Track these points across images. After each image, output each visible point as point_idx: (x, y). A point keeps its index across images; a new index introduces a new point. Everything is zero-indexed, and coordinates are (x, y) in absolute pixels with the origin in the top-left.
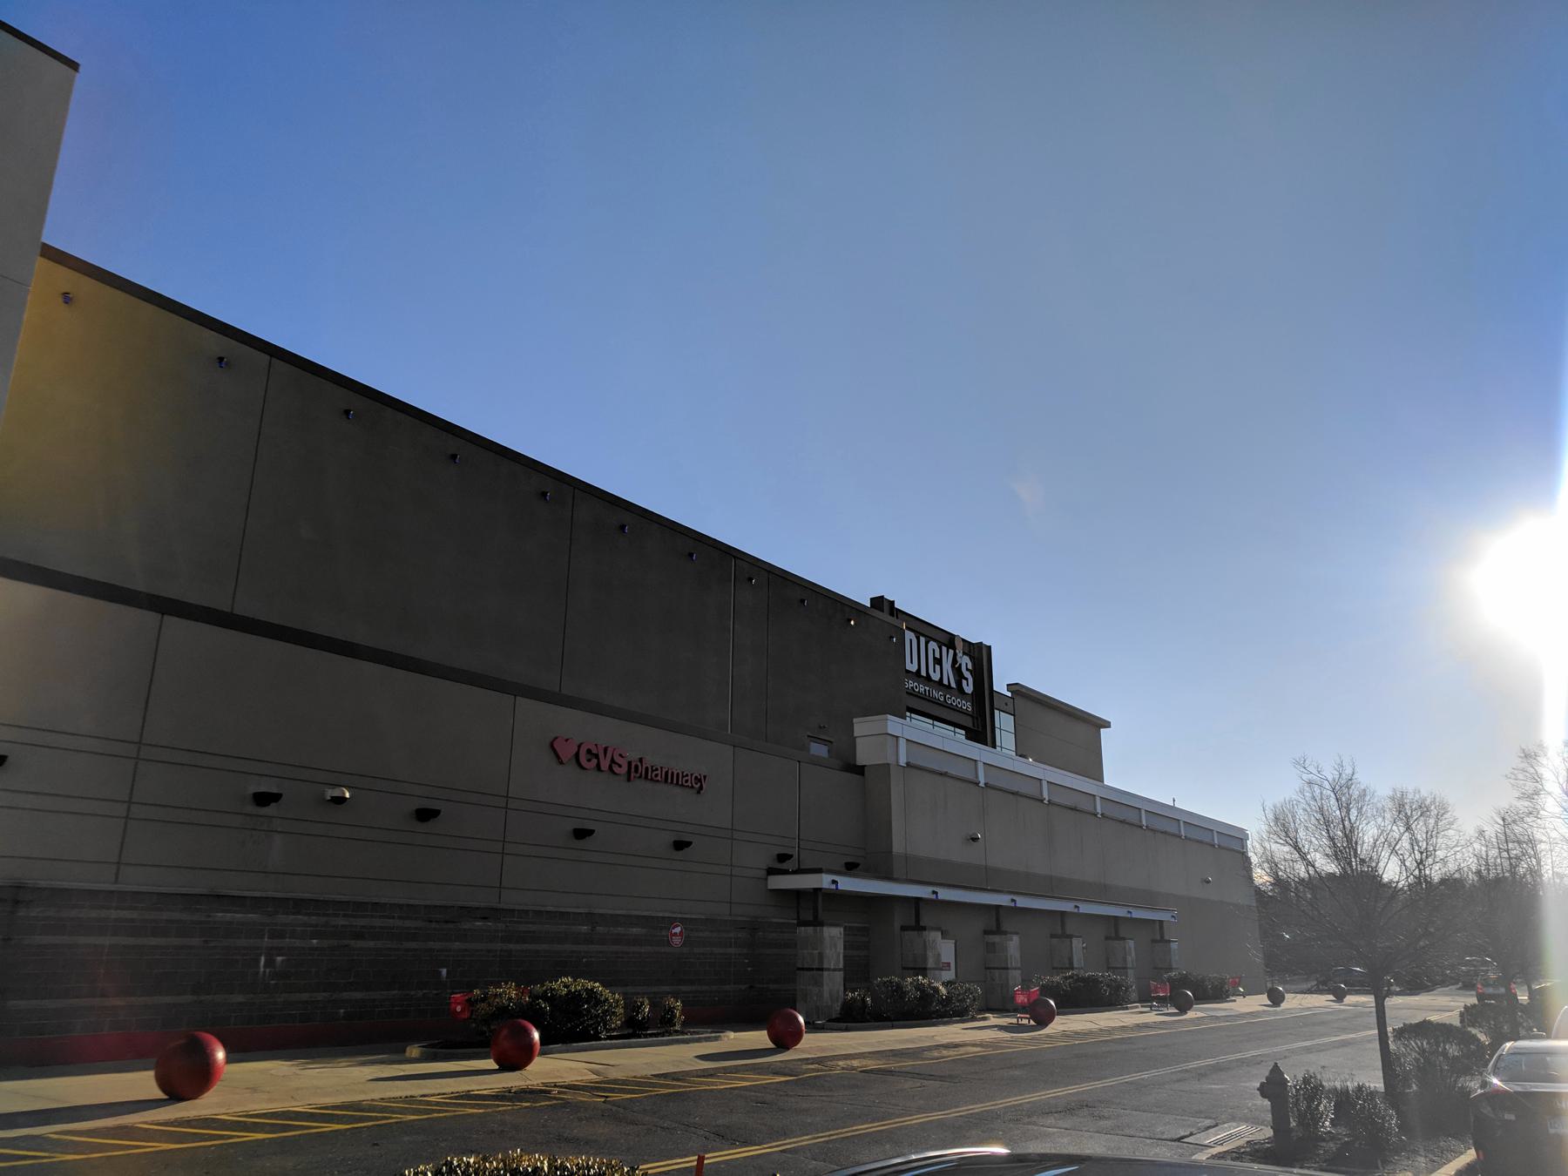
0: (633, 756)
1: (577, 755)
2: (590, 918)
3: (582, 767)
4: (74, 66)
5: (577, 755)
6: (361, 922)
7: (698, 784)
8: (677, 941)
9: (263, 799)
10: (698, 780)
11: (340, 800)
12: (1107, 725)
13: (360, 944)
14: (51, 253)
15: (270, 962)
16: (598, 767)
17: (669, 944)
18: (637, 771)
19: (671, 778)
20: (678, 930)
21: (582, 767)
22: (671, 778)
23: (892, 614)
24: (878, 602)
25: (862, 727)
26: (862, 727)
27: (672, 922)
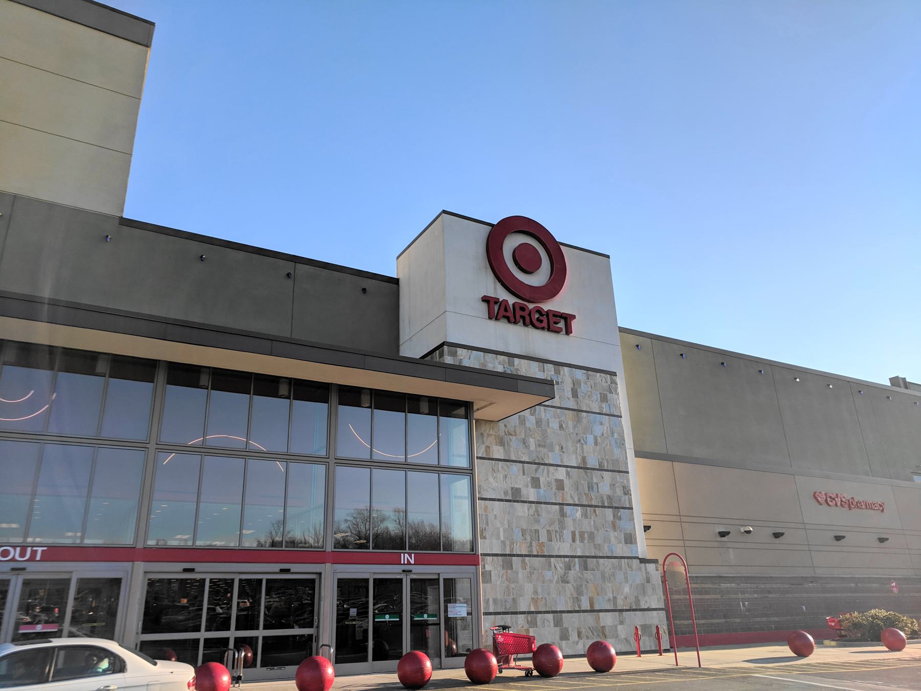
0: (849, 497)
1: (826, 500)
2: (852, 579)
3: (829, 505)
4: (608, 257)
5: (826, 500)
6: (768, 586)
7: (881, 508)
8: (895, 590)
9: (723, 534)
10: (881, 506)
11: (749, 532)
12: (574, 317)
13: (771, 596)
14: (622, 330)
15: (744, 605)
16: (836, 505)
17: (892, 592)
18: (850, 504)
19: (869, 506)
20: (894, 584)
21: (829, 505)
22: (869, 506)
23: (906, 388)
24: (895, 381)
25: (357, 638)
26: (357, 638)
27: (889, 580)
